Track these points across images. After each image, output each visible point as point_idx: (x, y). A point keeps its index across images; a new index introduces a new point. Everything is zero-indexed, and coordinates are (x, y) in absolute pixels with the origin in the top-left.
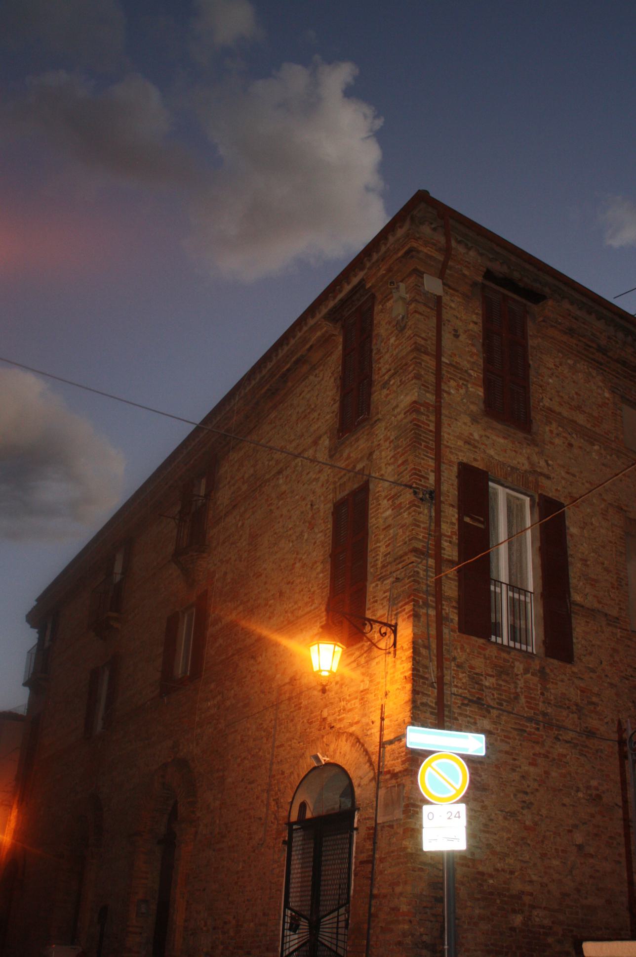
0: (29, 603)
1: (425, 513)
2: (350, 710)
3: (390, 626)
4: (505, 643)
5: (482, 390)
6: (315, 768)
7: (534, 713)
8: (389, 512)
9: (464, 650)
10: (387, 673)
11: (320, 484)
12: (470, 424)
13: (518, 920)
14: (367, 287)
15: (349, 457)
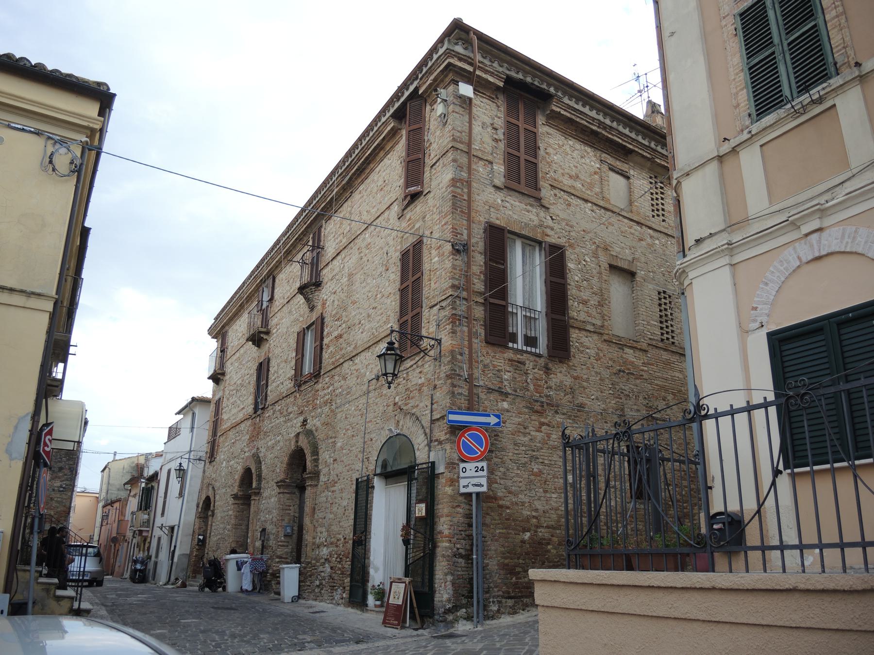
1: (460, 261)
2: (413, 398)
3: (436, 340)
4: (520, 348)
6: (390, 437)
8: (437, 259)
9: (672, 288)
13: (527, 535)
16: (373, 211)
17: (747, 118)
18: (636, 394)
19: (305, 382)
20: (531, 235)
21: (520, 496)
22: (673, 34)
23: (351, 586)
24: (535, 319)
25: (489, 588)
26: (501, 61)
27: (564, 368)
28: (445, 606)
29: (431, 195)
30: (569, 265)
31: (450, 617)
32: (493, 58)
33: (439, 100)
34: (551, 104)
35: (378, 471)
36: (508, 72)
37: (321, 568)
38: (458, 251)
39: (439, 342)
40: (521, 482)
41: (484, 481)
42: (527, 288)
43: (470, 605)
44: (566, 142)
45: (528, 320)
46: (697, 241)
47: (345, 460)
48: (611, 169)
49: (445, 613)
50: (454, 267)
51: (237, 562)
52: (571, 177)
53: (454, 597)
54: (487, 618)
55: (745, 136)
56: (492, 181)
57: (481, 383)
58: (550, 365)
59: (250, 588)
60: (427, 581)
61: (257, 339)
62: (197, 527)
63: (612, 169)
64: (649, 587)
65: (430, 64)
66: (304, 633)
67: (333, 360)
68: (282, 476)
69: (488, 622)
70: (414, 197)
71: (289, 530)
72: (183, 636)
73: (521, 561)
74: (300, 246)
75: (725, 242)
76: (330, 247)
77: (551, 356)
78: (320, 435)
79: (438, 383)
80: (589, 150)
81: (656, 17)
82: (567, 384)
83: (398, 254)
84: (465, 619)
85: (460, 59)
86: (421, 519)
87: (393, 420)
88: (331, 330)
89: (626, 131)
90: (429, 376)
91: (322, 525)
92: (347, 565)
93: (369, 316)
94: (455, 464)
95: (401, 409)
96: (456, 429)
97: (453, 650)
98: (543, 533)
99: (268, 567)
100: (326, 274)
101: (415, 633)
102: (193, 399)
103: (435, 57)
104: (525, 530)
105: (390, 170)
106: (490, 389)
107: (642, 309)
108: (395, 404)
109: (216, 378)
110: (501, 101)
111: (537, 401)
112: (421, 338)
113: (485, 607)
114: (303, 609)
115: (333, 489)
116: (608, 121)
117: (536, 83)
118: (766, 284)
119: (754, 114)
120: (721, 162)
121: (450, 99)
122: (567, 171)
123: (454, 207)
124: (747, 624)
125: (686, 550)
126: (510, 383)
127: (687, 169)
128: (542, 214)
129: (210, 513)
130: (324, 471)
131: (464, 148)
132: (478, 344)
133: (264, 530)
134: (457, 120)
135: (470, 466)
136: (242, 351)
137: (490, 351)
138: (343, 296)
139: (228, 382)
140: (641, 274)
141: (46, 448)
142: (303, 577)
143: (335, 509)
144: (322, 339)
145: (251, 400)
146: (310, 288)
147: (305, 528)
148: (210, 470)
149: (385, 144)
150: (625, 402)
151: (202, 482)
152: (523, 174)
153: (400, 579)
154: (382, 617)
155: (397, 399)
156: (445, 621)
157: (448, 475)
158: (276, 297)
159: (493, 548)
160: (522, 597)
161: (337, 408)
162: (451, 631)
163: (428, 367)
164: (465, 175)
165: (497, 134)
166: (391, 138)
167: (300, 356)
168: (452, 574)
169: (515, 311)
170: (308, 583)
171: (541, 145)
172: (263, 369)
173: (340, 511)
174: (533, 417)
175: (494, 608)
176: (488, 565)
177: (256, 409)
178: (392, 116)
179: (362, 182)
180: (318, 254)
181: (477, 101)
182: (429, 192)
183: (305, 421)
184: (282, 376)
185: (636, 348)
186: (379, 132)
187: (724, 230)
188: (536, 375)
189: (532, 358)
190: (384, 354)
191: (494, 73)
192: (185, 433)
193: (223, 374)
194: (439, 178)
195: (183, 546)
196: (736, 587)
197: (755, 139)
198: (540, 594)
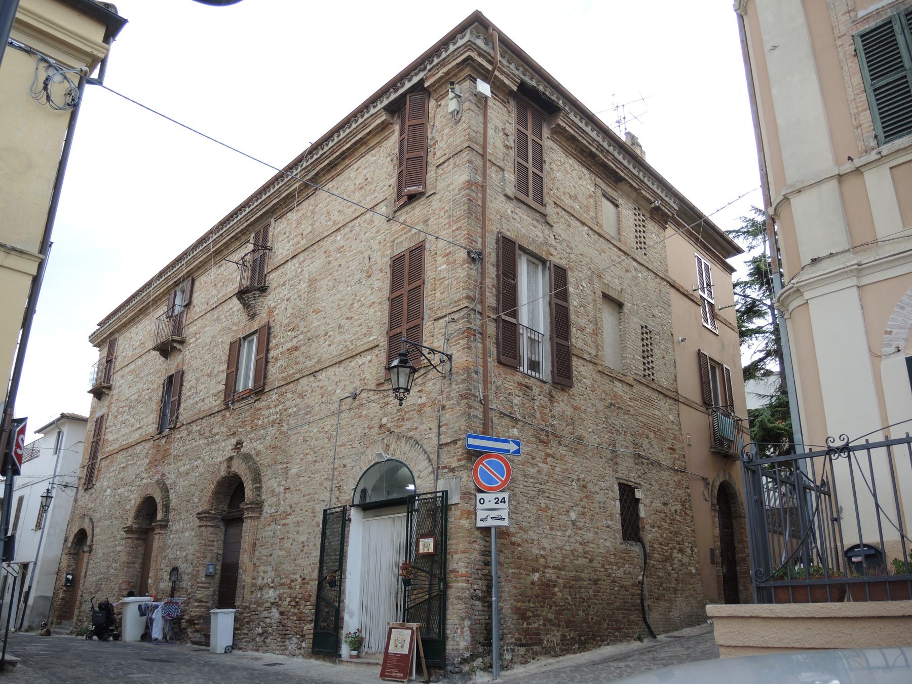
2: (408, 419)
3: (447, 355)
4: (526, 371)
11: (377, 241)
17: (871, 139)
20: (537, 252)
22: (774, 48)
29: (437, 197)
31: (466, 668)
33: (451, 95)
34: (556, 117)
35: (357, 502)
36: (523, 77)
37: (265, 614)
39: (450, 357)
40: (530, 517)
41: (505, 514)
45: (532, 341)
46: (814, 261)
47: (299, 489)
48: (604, 195)
49: (461, 663)
50: (469, 277)
51: (140, 606)
53: (472, 644)
54: (504, 668)
55: (873, 156)
57: (494, 406)
58: (554, 393)
59: (160, 637)
63: (604, 195)
65: (444, 55)
67: (285, 374)
68: (206, 507)
69: (503, 673)
71: (211, 570)
73: (532, 605)
77: (555, 383)
78: (263, 461)
79: (448, 404)
80: (586, 172)
81: (740, 31)
82: (569, 414)
83: (387, 260)
85: (480, 55)
88: (281, 342)
92: (308, 610)
93: (340, 327)
94: (471, 494)
96: (474, 455)
98: (550, 574)
102: (63, 416)
103: (452, 48)
104: (535, 570)
106: (501, 413)
108: (381, 426)
109: (99, 392)
111: (543, 430)
115: (283, 522)
116: (605, 145)
117: (547, 93)
118: (903, 308)
119: (882, 136)
122: (567, 190)
123: (470, 211)
128: (547, 232)
129: (86, 549)
132: (492, 362)
134: (471, 118)
135: (489, 497)
136: (139, 362)
137: (501, 372)
139: (115, 397)
140: (628, 305)
141: (18, 450)
142: (239, 624)
144: (268, 351)
146: (251, 292)
148: (85, 499)
149: (370, 139)
150: (616, 437)
151: (73, 512)
152: (531, 189)
156: (460, 672)
158: (195, 301)
159: (507, 589)
160: (532, 644)
164: (479, 179)
167: (234, 369)
168: (470, 619)
170: (245, 631)
172: (173, 385)
175: (508, 657)
177: (160, 430)
178: (385, 108)
179: (333, 178)
182: (434, 193)
184: (203, 390)
187: (848, 251)
188: (542, 402)
189: (539, 383)
194: (448, 180)
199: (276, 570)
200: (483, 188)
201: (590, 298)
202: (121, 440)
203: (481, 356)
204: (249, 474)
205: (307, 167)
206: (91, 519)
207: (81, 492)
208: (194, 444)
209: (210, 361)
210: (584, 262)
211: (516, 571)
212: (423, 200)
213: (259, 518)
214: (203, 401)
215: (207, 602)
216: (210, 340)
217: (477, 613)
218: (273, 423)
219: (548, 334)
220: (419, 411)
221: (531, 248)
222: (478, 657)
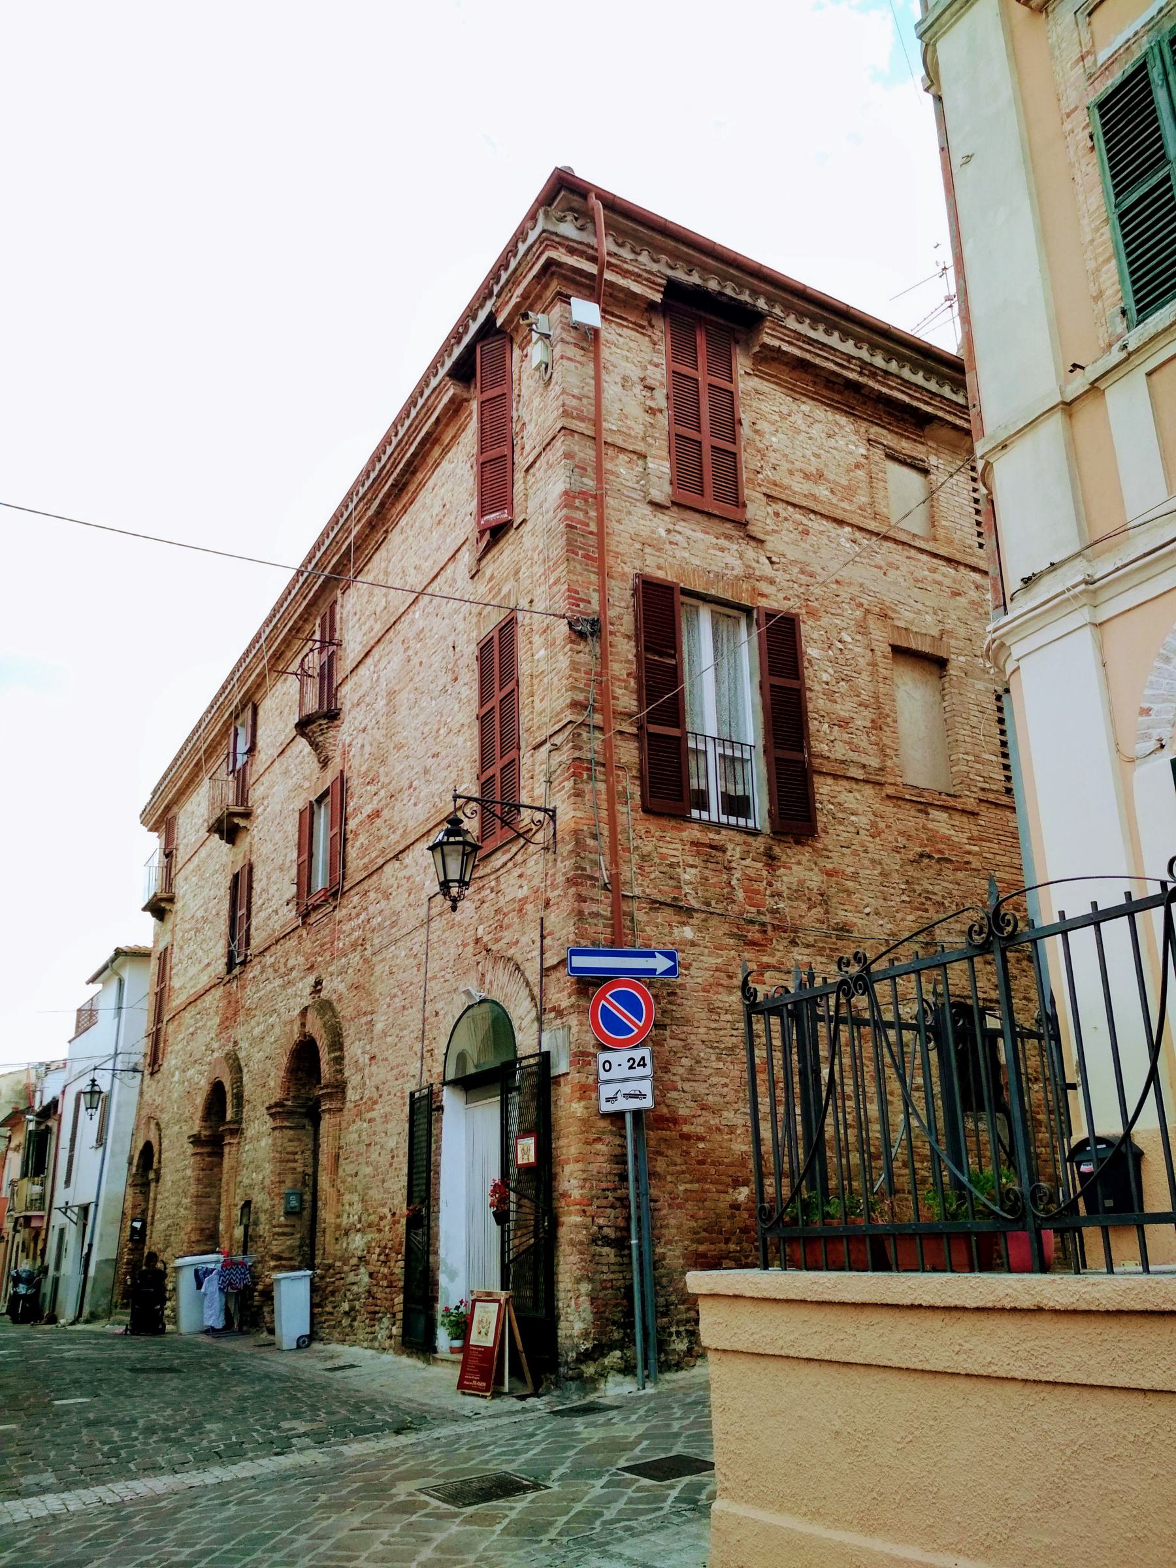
0: (144, 798)
1: (586, 654)
2: (509, 926)
3: (546, 811)
4: (714, 818)
5: (668, 464)
6: (469, 1007)
7: (759, 912)
8: (542, 652)
10: (546, 875)
11: (461, 616)
12: (651, 517)
14: (498, 324)
15: (492, 578)
16: (426, 565)
18: (958, 899)
19: (316, 908)
20: (728, 596)
21: (725, 1114)
23: (406, 1311)
24: (743, 761)
25: (668, 1304)
26: (656, 250)
27: (805, 855)
28: (577, 1346)
30: (809, 651)
31: (590, 1370)
32: (640, 244)
33: (535, 336)
36: (669, 272)
37: (352, 1278)
38: (582, 635)
39: (552, 814)
40: (725, 1085)
41: (646, 1087)
42: (725, 701)
43: (625, 1343)
44: (794, 407)
45: (729, 762)
46: (1027, 581)
48: (890, 457)
50: (575, 667)
51: (196, 1271)
52: (807, 476)
54: (665, 1367)
55: (1116, 356)
56: (647, 493)
57: (637, 891)
58: (777, 850)
59: (219, 1324)
60: (542, 1295)
61: (228, 828)
62: (129, 1204)
64: (912, 1307)
66: (296, 1415)
67: (366, 860)
68: (278, 1095)
69: (668, 1376)
70: (496, 534)
71: (294, 1202)
72: (48, 1436)
73: (732, 1247)
74: (298, 643)
75: (1080, 578)
76: (353, 641)
78: (345, 1010)
79: (552, 894)
80: (843, 420)
82: (814, 885)
84: (620, 1371)
85: (572, 251)
86: (526, 1169)
87: (473, 973)
88: (361, 803)
89: (919, 379)
90: (536, 882)
91: (353, 1190)
92: (399, 1267)
93: (426, 771)
95: (488, 951)
97: (583, 1440)
99: (256, 1279)
100: (347, 695)
101: (519, 1405)
102: (118, 953)
104: (737, 1183)
105: (453, 480)
106: (655, 902)
107: (963, 732)
110: (660, 329)
111: (752, 922)
112: (518, 807)
113: (662, 1346)
114: (310, 1365)
115: (369, 1115)
116: (879, 361)
120: (1070, 416)
121: (556, 332)
122: (798, 465)
124: (1112, 1388)
125: (985, 1225)
126: (695, 890)
127: (1003, 436)
129: (152, 1175)
130: (353, 1079)
131: (588, 430)
132: (628, 814)
133: (247, 1204)
134: (572, 374)
135: (619, 1058)
136: (203, 852)
137: (652, 828)
138: (379, 735)
139: (180, 915)
140: (957, 662)
142: (319, 1295)
143: (374, 1156)
144: (344, 820)
145: (219, 949)
146: (316, 724)
147: (321, 1195)
148: (151, 1087)
149: (442, 433)
151: (138, 1114)
152: (709, 477)
153: (489, 1294)
154: (458, 1373)
155: (480, 932)
156: (580, 1377)
157: (575, 1077)
158: (260, 743)
159: (673, 1222)
161: (374, 954)
162: (592, 1397)
163: (535, 863)
164: (590, 483)
165: (652, 398)
166: (451, 420)
167: (305, 856)
168: (590, 1280)
169: (701, 747)
170: (329, 1309)
171: (745, 417)
172: (241, 887)
173: (384, 1159)
174: (746, 955)
176: (663, 1257)
177: (230, 965)
179: (405, 510)
180: (331, 658)
181: (609, 333)
182: (524, 521)
183: (318, 983)
185: (954, 809)
186: (428, 409)
187: (1078, 555)
188: (749, 871)
189: (739, 838)
190: (440, 844)
191: (643, 273)
192: (106, 1018)
193: (171, 900)
194: (541, 493)
195: (106, 1243)
196: (1084, 1307)
197: (1135, 360)
198: (713, 1326)
199: (363, 1201)
200: (598, 500)
201: (862, 662)
202: (188, 986)
203: (604, 805)
204: (324, 1036)
205: (365, 495)
206: (157, 1124)
207: (147, 1077)
208: (269, 987)
209: (281, 843)
210: (845, 596)
211: (696, 1186)
212: (512, 535)
213: (341, 1110)
214: (276, 912)
215: (291, 1259)
216: (279, 807)
217: (605, 1269)
218: (354, 946)
219: (760, 743)
220: (520, 910)
221: (713, 592)
222: (612, 1347)
